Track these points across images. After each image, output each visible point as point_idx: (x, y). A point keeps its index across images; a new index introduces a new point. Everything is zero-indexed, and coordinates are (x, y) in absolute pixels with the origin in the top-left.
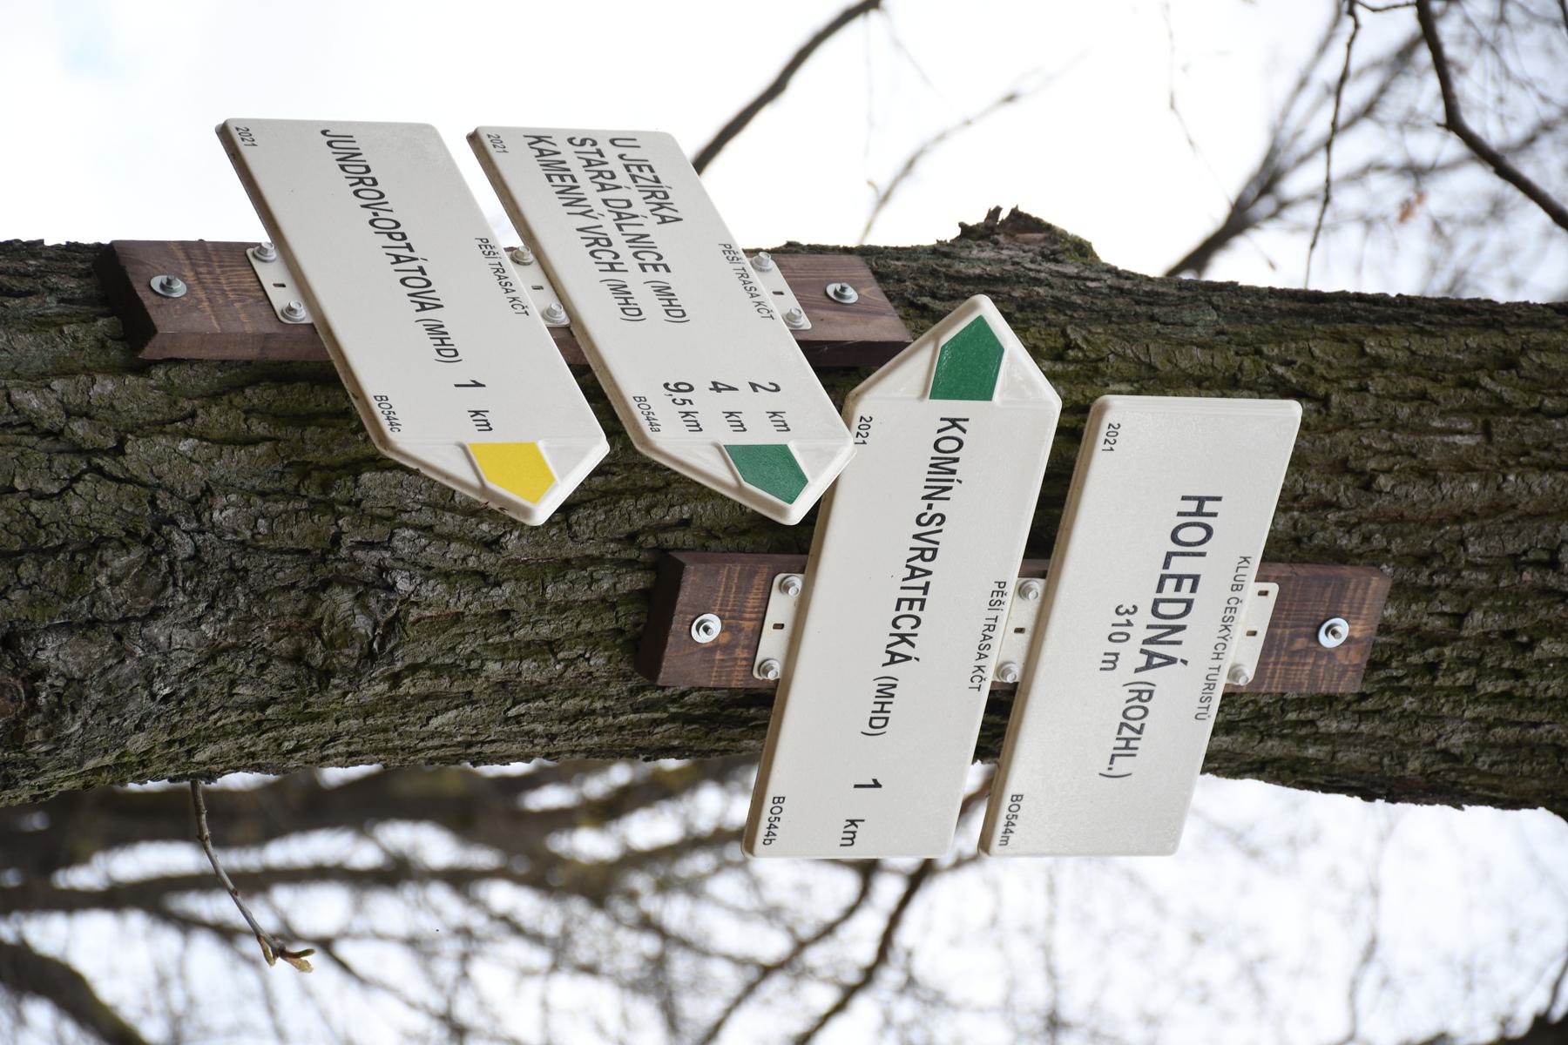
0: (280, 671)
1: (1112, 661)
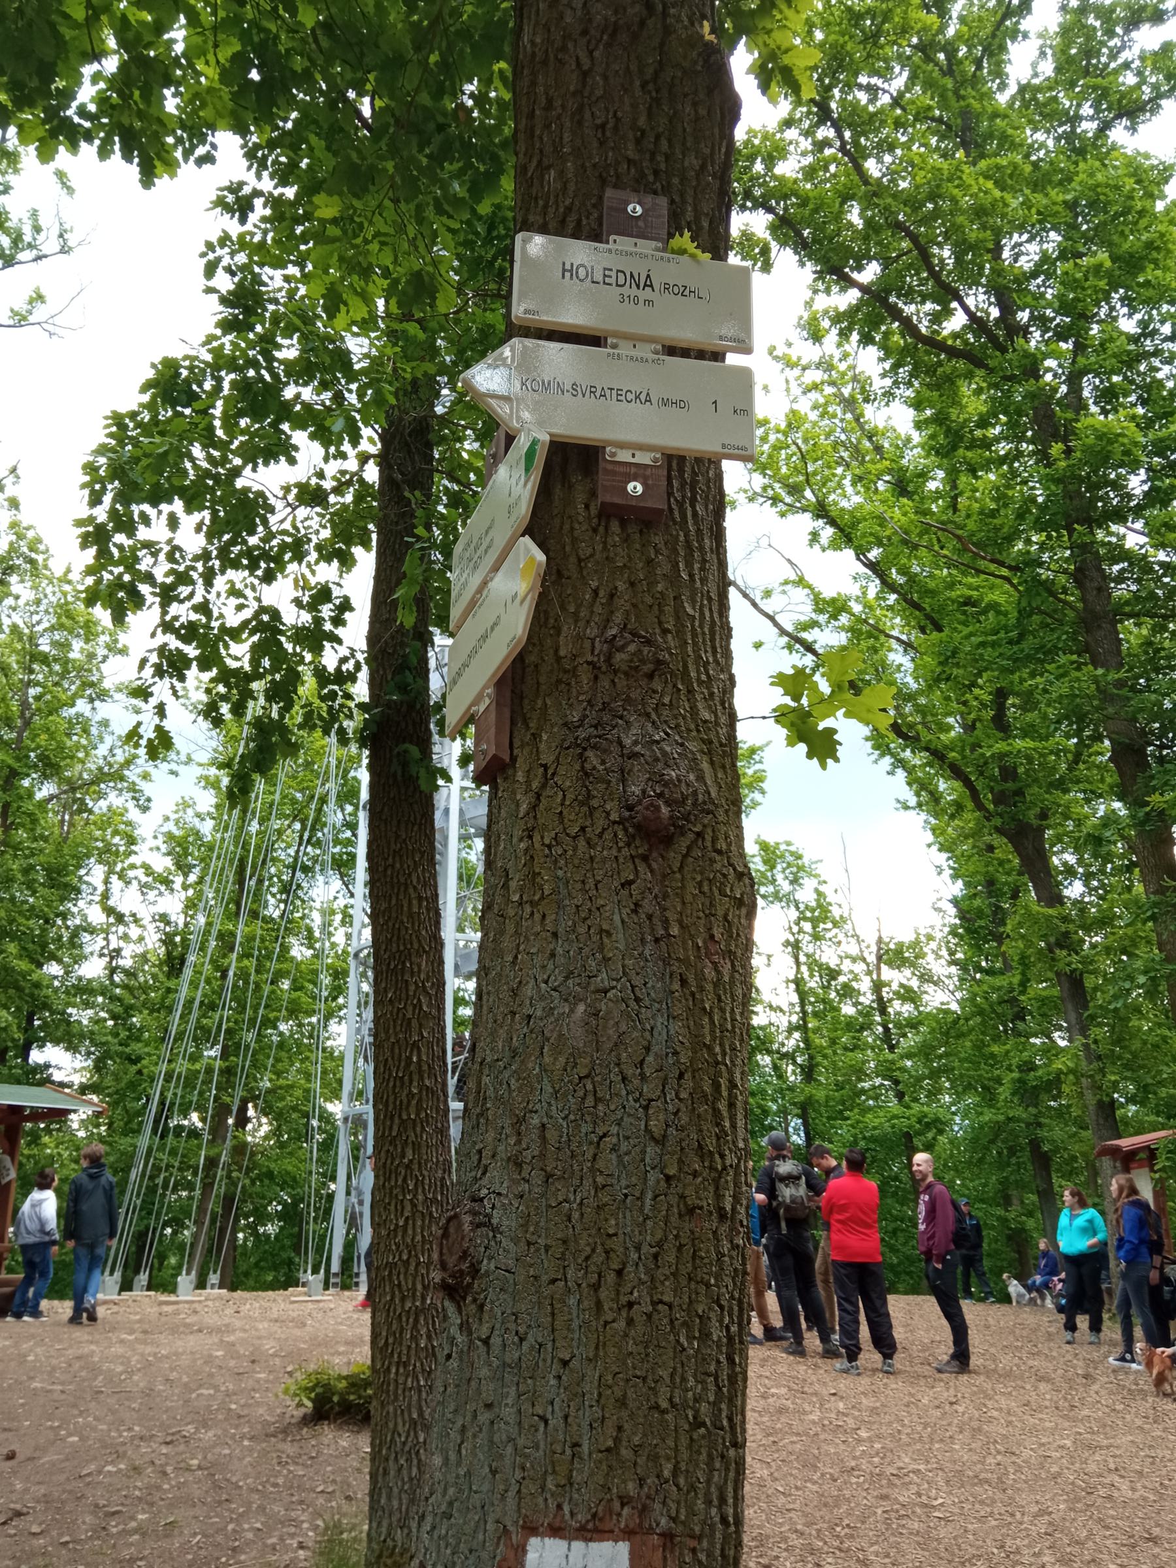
0: (657, 685)
1: (648, 302)
